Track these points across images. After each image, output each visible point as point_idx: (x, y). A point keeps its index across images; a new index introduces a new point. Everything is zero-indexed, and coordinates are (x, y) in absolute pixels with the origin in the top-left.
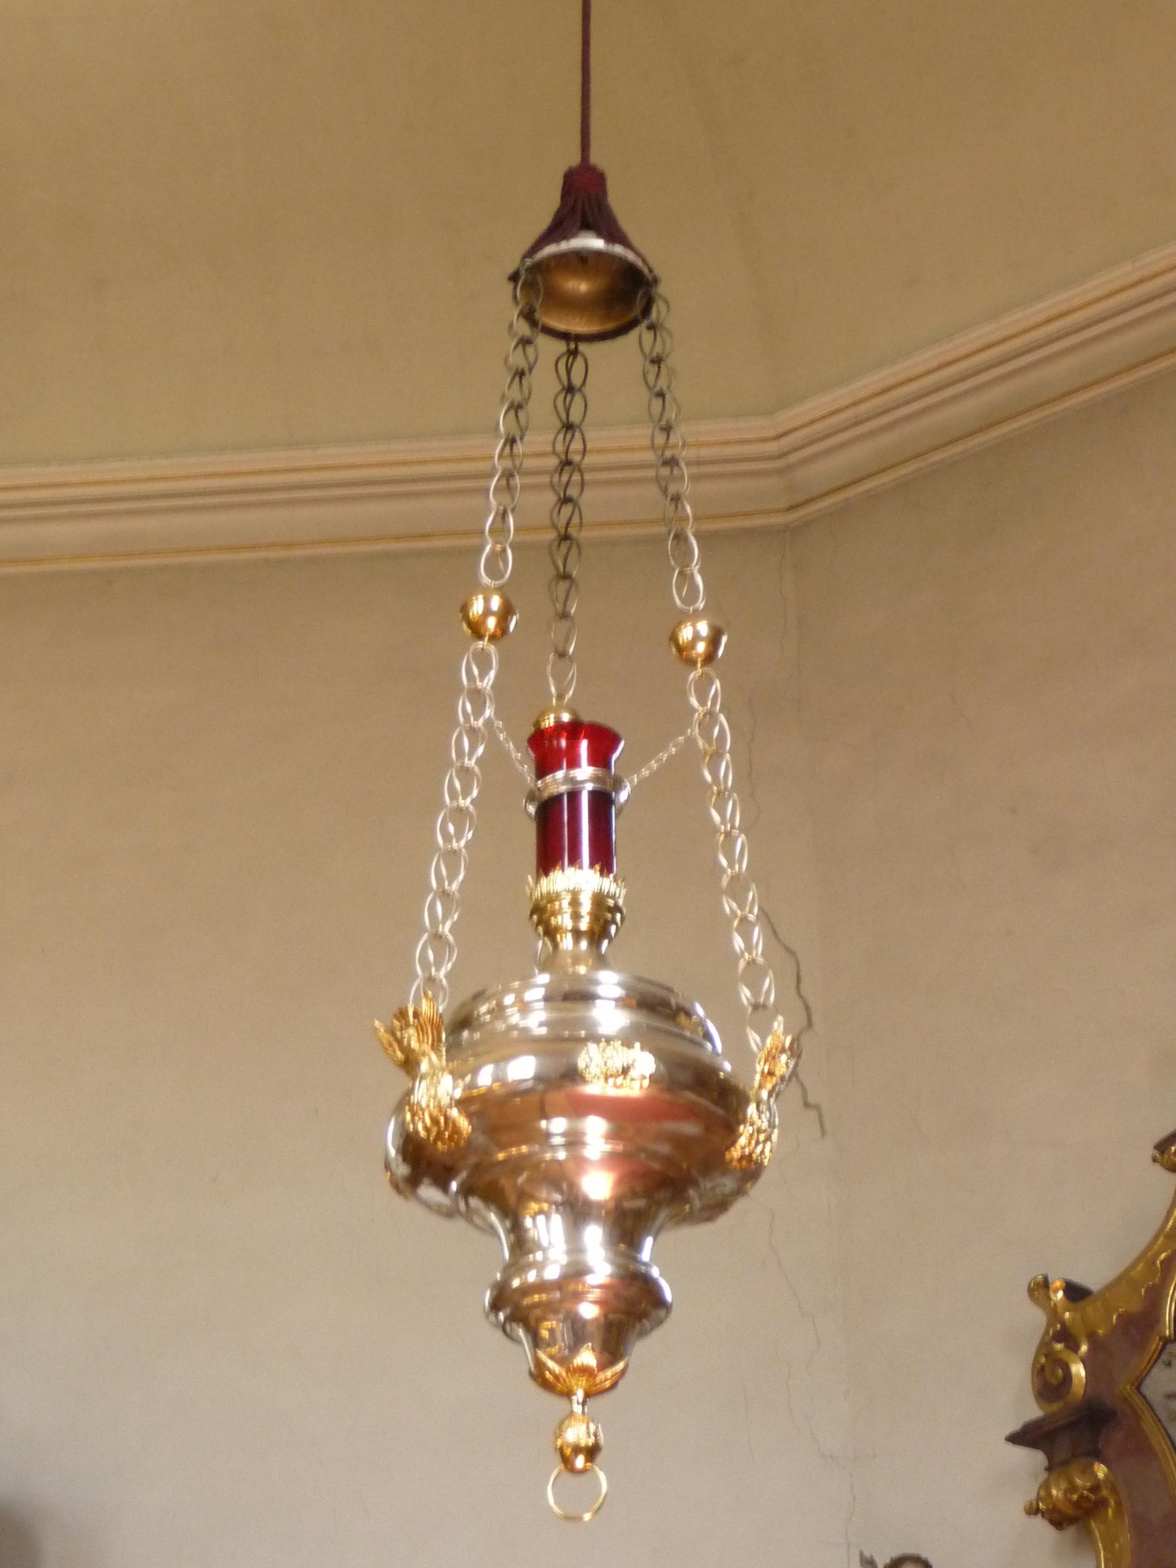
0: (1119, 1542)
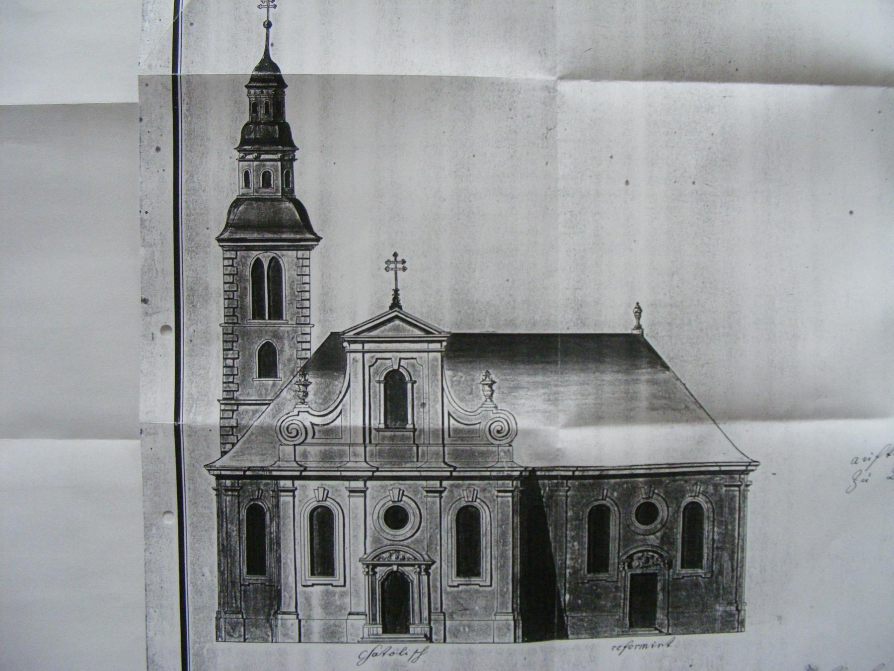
0: (616, 357)
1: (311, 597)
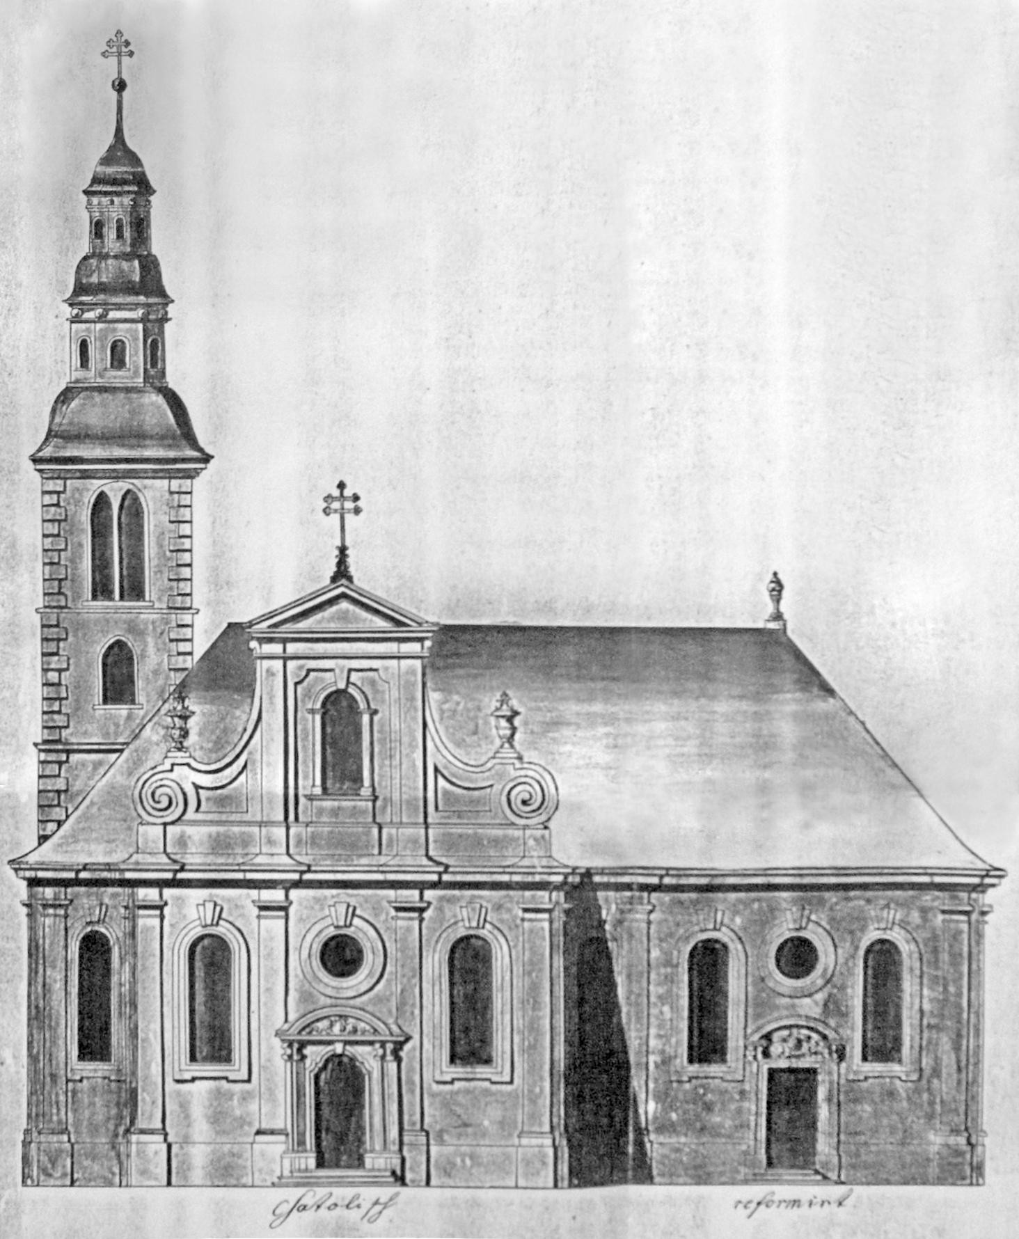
1: (189, 1102)
